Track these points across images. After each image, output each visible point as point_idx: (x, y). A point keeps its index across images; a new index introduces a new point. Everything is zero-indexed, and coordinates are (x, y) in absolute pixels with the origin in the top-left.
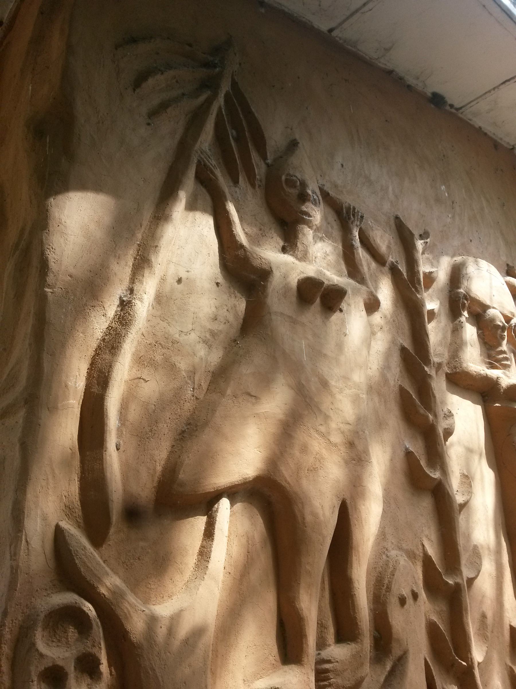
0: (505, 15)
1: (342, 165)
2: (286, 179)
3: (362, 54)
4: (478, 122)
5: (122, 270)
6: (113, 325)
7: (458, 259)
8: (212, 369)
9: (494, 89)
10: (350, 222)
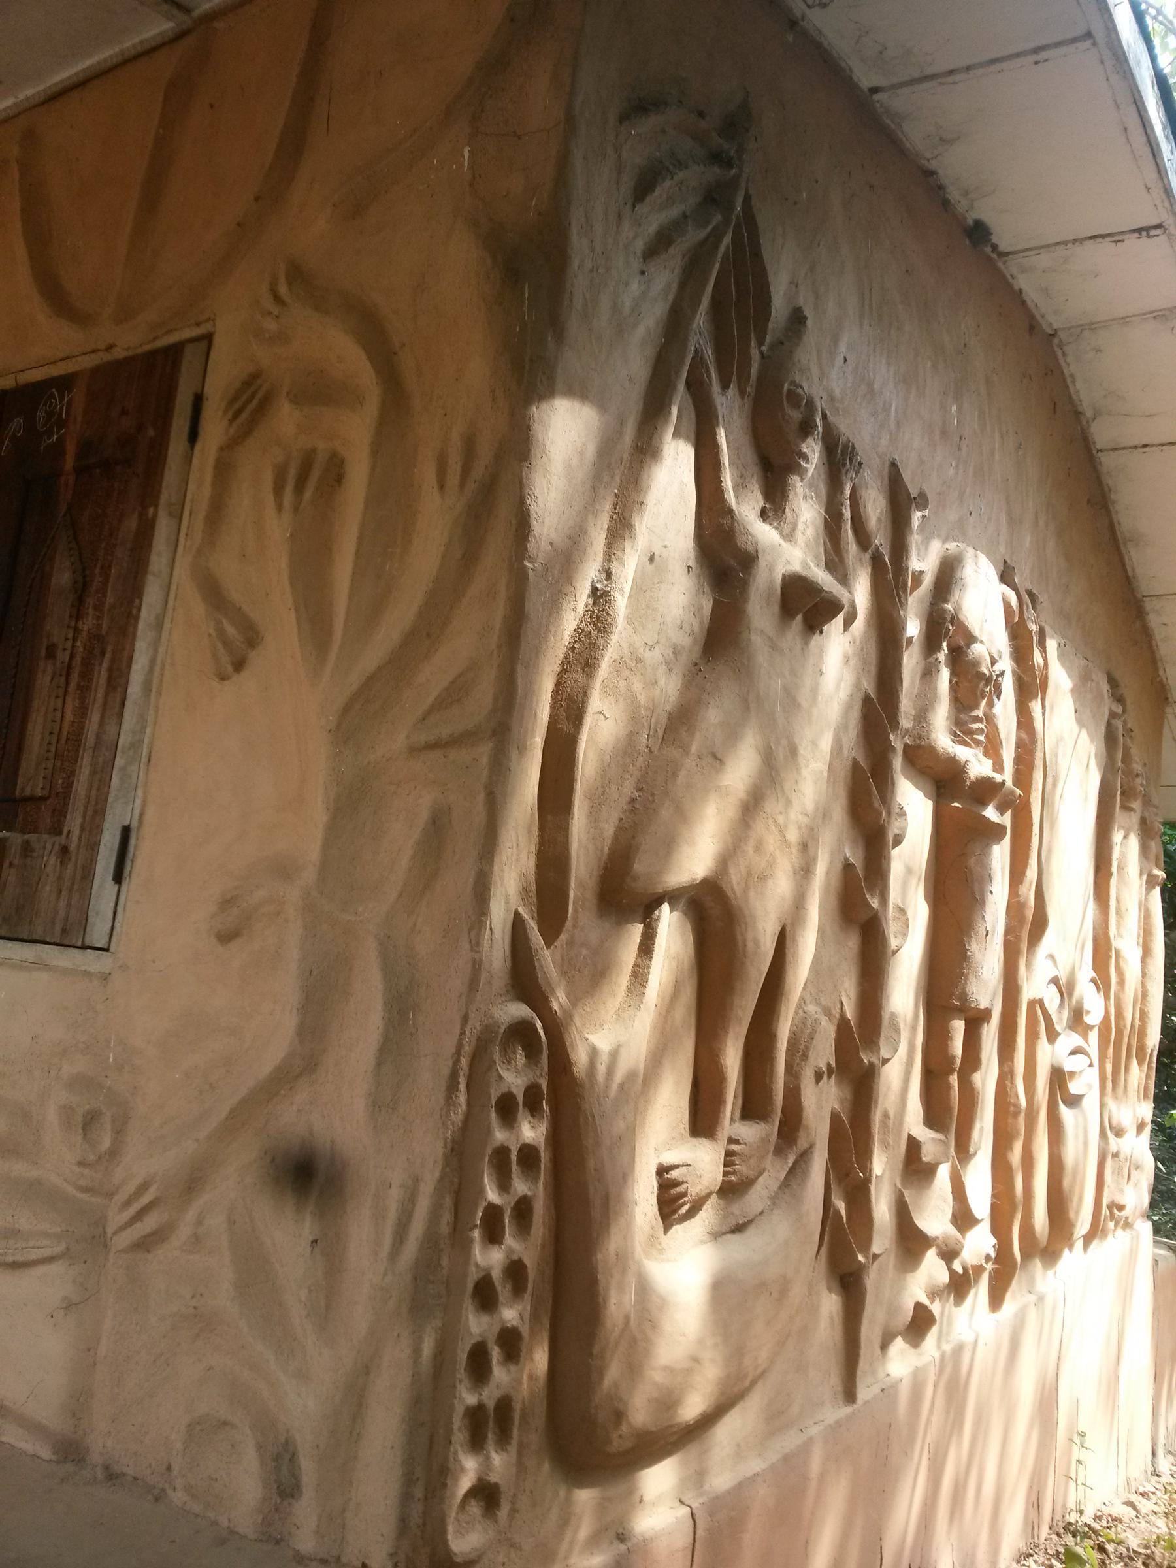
0: (1148, 149)
1: (845, 360)
2: (789, 390)
3: (901, 136)
4: (1023, 282)
5: (598, 539)
6: (583, 626)
7: (952, 546)
8: (669, 708)
9: (1075, 241)
10: (844, 472)
